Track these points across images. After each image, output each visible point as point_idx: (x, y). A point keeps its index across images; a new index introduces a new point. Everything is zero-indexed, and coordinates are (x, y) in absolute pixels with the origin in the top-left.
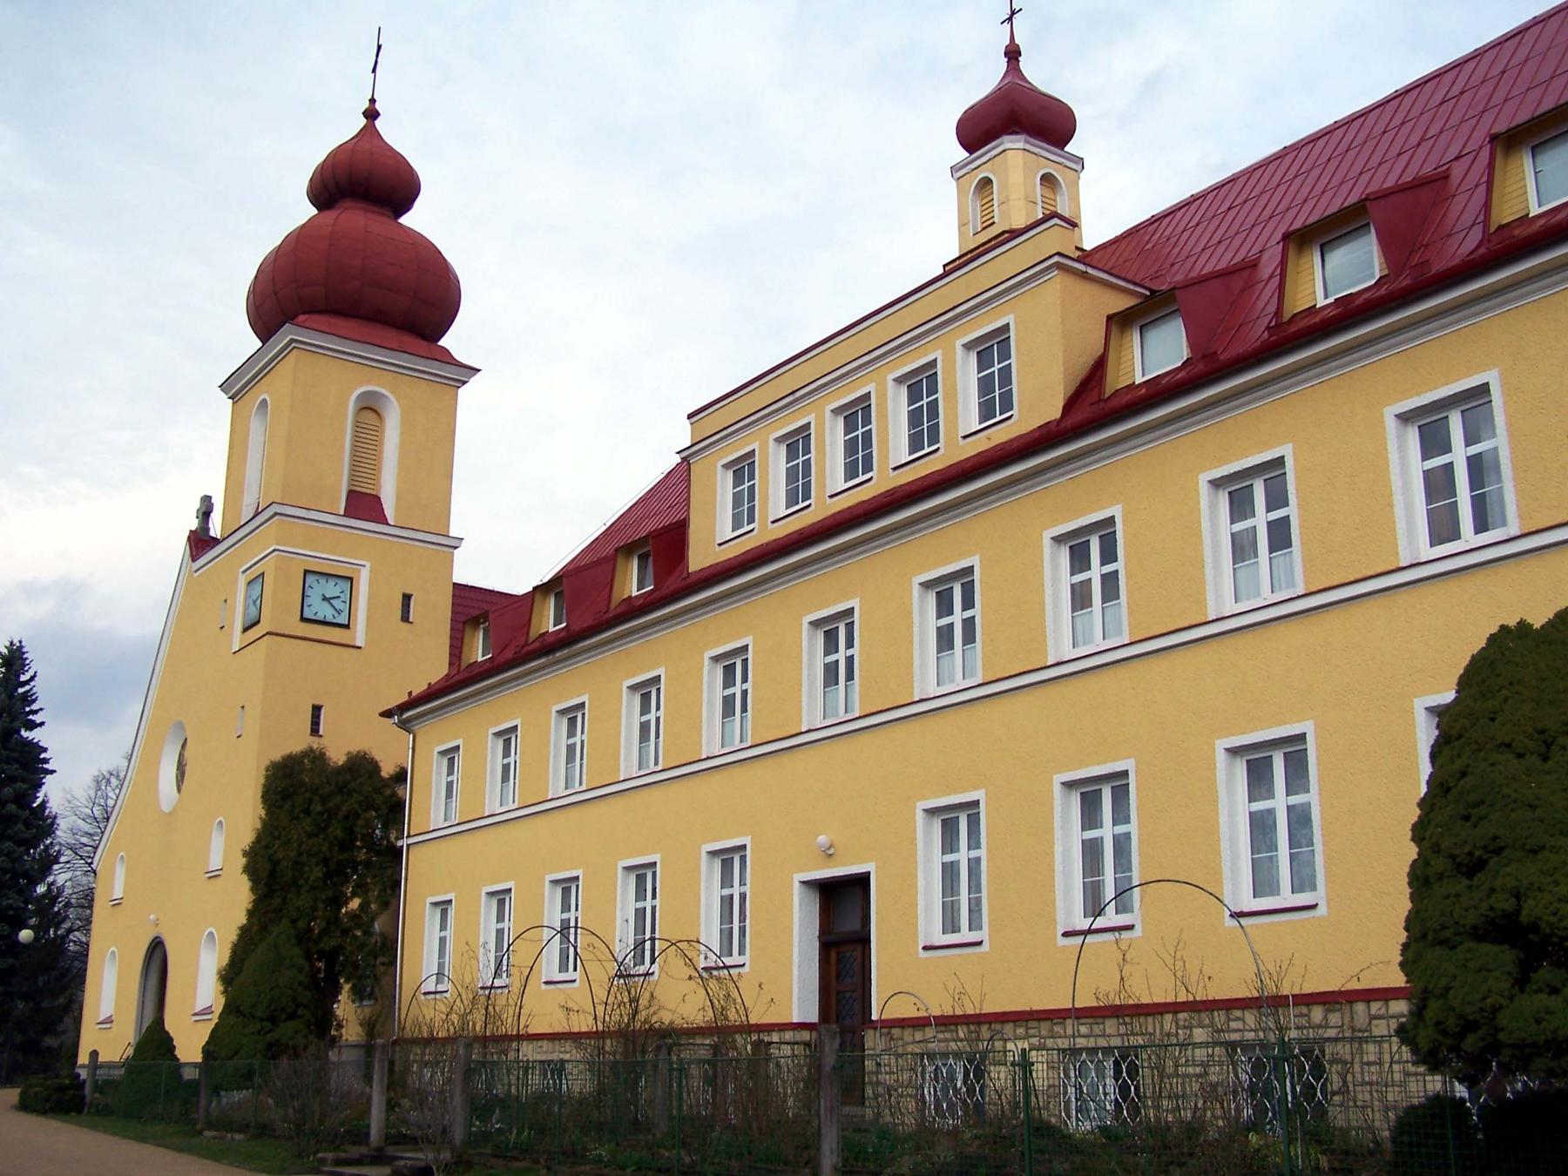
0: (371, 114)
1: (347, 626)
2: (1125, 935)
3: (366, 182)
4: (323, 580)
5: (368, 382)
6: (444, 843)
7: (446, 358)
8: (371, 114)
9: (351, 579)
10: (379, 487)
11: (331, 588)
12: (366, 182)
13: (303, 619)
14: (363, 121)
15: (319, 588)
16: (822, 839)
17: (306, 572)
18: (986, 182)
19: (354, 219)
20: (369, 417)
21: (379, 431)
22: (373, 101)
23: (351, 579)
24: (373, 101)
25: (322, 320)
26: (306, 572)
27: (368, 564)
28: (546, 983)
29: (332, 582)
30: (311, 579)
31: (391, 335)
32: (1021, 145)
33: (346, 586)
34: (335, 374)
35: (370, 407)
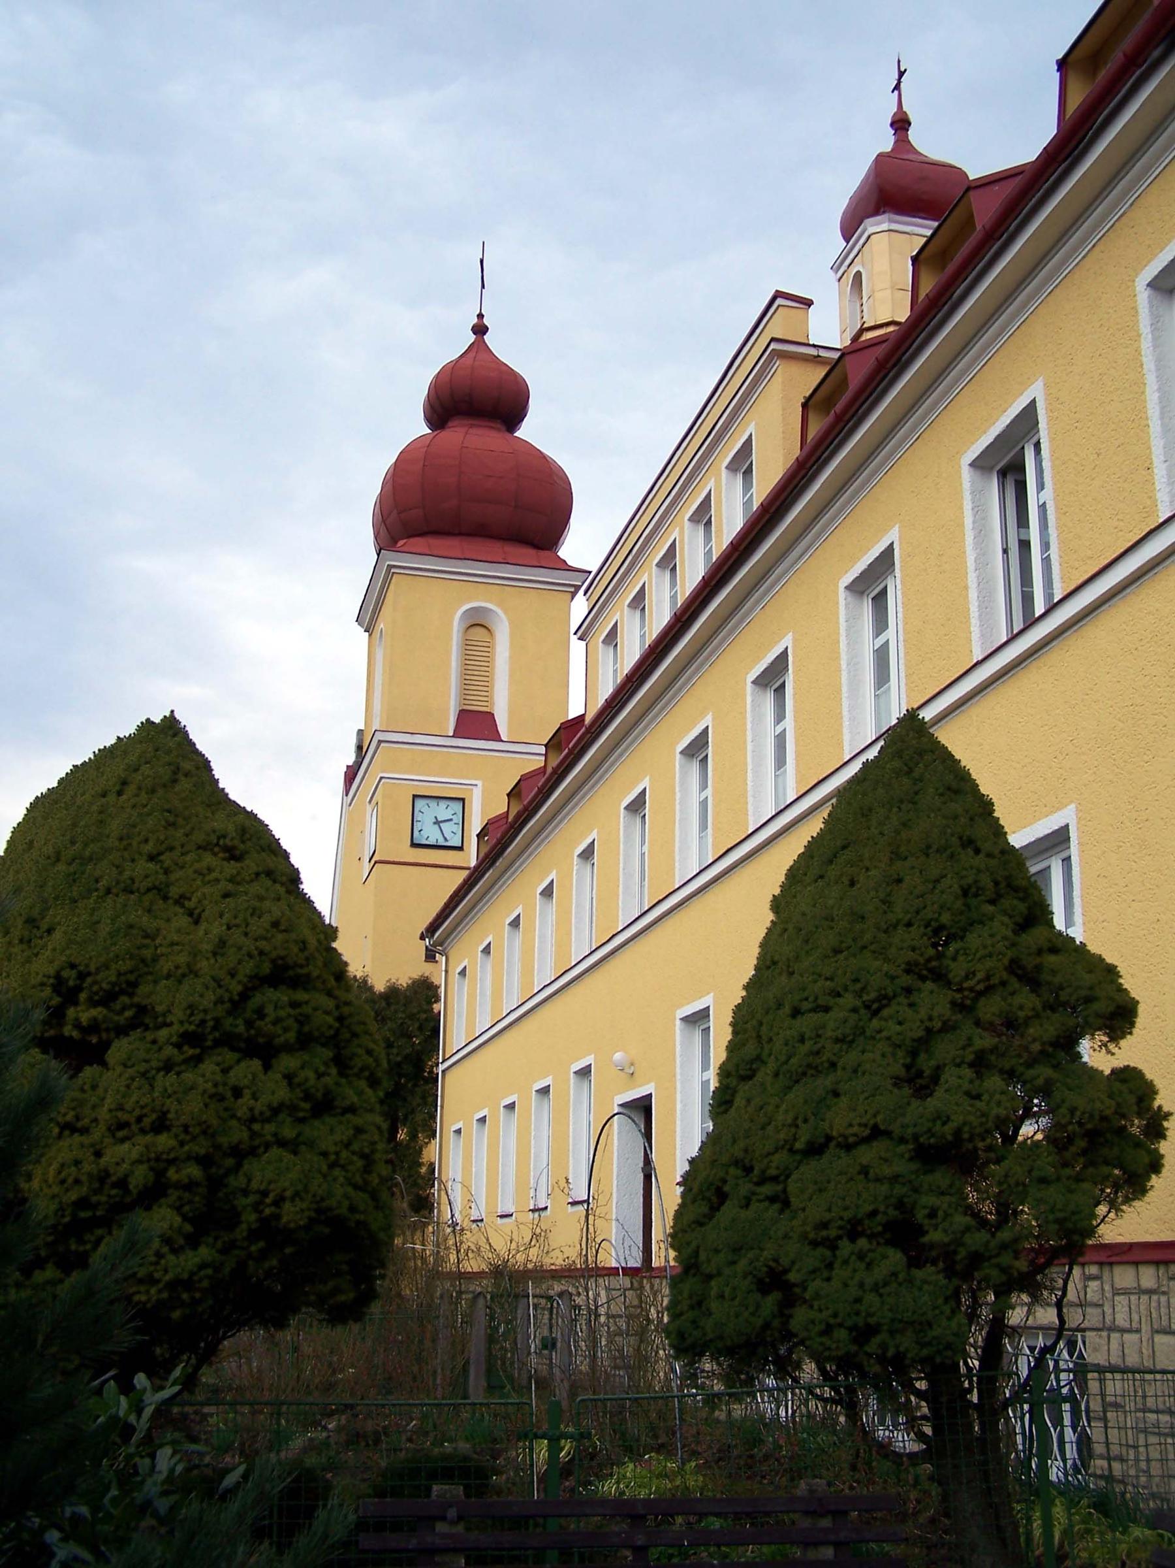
0: (480, 330)
1: (461, 848)
2: (543, 1214)
3: (476, 398)
4: (433, 803)
5: (469, 600)
6: (466, 1063)
7: (564, 566)
8: (480, 330)
9: (463, 800)
10: (493, 704)
11: (443, 811)
12: (476, 398)
13: (414, 845)
14: (472, 338)
15: (428, 812)
16: (618, 1056)
17: (415, 797)
18: (858, 275)
19: (471, 439)
20: (479, 633)
21: (490, 647)
22: (481, 316)
23: (463, 800)
24: (481, 316)
25: (419, 543)
26: (415, 797)
27: (479, 783)
28: (502, 1216)
29: (443, 804)
30: (420, 803)
31: (497, 548)
32: (885, 226)
33: (457, 807)
34: (449, 591)
35: (477, 623)
